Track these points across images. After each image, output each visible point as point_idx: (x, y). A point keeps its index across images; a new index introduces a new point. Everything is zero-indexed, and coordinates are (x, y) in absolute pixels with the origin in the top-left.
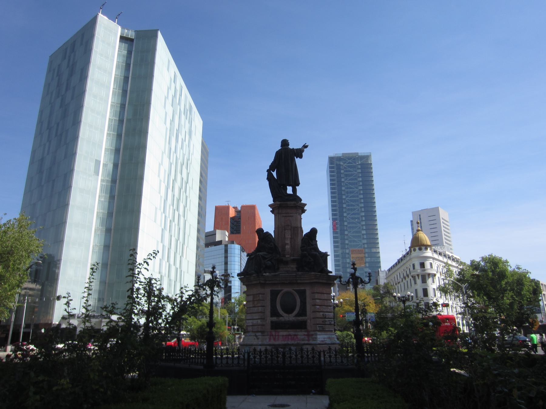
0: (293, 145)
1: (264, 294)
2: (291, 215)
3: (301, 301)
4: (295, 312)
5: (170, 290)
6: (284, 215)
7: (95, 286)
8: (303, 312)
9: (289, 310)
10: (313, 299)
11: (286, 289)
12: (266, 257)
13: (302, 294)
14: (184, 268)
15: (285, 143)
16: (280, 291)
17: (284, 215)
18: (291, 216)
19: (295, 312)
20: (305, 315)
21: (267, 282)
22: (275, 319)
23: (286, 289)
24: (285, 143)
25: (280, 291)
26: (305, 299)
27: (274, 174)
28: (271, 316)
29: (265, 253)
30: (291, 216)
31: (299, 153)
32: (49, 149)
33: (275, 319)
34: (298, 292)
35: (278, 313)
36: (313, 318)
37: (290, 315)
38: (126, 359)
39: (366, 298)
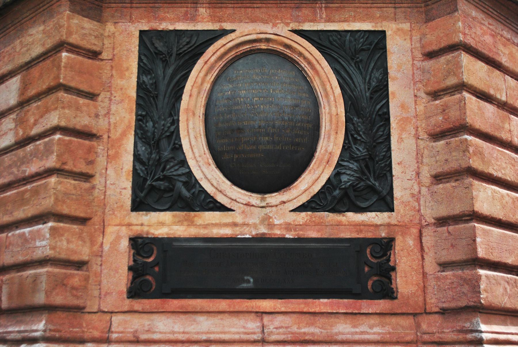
1: (94, 55)
3: (352, 105)
4: (313, 180)
7: (276, 237)
8: (365, 180)
9: (263, 161)
11: (245, 30)
13: (360, 59)
19: (313, 180)
20: (386, 203)
22: (163, 224)
26: (382, 90)
28: (139, 205)
32: (512, 334)
33: (163, 224)
34: (197, 201)
35: (190, 181)
36: (442, 221)
37: (274, 198)
38: (366, 269)
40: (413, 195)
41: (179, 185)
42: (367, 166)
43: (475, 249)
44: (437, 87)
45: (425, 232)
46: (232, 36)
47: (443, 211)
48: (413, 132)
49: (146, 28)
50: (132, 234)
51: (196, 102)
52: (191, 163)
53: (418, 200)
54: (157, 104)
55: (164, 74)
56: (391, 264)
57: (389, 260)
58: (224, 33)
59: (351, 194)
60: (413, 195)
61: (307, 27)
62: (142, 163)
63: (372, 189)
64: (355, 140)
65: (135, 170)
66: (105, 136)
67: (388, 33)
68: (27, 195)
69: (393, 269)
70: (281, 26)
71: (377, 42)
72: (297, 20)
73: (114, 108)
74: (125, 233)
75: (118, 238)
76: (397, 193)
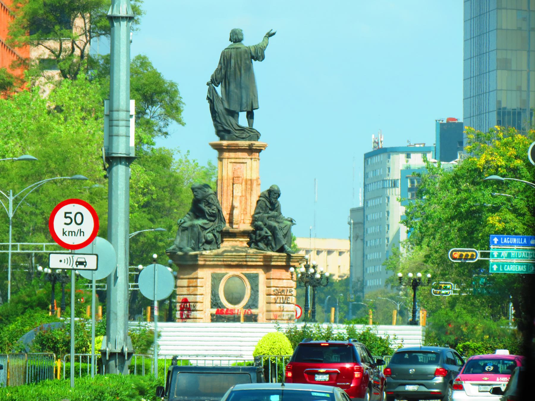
0: (250, 41)
2: (244, 161)
3: (252, 288)
4: (244, 302)
5: (201, 164)
6: (233, 161)
10: (268, 287)
12: (206, 227)
13: (253, 279)
14: (225, 188)
15: (236, 37)
16: (223, 275)
17: (233, 161)
18: (243, 163)
19: (244, 302)
21: (208, 263)
23: (231, 272)
24: (236, 37)
25: (223, 275)
26: (257, 285)
27: (219, 89)
29: (205, 221)
30: (243, 163)
31: (258, 55)
34: (248, 276)
39: (18, 188)
61: (243, 272)
71: (256, 276)
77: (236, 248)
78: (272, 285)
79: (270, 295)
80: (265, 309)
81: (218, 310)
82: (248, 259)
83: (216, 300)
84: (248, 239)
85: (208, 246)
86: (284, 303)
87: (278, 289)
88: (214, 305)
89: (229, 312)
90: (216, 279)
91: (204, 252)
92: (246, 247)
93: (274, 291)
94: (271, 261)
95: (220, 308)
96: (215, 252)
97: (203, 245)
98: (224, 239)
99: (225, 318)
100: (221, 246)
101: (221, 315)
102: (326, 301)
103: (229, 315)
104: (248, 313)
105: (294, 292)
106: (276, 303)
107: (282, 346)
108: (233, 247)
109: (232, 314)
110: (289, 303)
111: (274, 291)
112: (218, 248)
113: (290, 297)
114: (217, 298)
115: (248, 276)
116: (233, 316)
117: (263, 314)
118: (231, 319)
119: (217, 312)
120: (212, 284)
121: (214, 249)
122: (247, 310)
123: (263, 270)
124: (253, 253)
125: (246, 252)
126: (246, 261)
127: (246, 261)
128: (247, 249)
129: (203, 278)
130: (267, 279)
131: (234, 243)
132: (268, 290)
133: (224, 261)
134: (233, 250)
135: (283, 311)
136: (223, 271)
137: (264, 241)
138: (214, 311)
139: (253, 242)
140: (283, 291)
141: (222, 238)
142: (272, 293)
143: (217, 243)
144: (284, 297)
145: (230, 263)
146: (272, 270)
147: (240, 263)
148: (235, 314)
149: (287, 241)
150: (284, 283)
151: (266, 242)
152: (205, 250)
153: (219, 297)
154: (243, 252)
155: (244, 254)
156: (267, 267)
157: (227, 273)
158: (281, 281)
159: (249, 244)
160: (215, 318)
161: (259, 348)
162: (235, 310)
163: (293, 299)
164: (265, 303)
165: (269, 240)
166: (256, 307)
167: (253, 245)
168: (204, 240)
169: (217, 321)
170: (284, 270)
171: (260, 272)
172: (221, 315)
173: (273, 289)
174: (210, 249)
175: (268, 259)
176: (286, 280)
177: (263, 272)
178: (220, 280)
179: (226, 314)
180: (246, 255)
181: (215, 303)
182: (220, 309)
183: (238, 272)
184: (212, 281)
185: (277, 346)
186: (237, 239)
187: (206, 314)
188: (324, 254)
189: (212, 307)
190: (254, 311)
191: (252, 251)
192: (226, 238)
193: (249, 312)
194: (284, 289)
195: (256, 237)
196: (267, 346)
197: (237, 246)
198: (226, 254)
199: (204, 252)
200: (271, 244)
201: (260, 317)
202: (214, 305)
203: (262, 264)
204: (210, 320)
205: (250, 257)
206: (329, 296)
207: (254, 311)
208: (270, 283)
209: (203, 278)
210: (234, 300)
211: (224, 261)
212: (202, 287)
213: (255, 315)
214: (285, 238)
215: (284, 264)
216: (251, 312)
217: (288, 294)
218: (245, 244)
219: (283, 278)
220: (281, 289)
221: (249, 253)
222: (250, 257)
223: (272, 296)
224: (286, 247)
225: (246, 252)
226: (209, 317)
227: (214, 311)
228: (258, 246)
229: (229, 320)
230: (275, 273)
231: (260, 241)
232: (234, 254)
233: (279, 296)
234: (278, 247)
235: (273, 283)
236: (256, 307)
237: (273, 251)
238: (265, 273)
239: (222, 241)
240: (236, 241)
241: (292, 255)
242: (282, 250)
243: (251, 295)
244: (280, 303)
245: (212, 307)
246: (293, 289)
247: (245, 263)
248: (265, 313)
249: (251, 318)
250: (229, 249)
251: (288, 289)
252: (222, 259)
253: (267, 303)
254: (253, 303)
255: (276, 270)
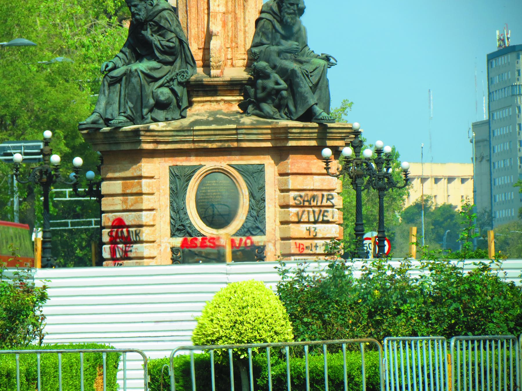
3: (252, 195)
13: (253, 176)
16: (194, 169)
23: (210, 163)
25: (194, 169)
26: (262, 188)
34: (242, 170)
40: (273, 229)
41: (187, 228)
42: (256, 219)
43: (290, 251)
44: (283, 188)
45: (277, 243)
46: (204, 167)
47: (283, 236)
48: (274, 205)
49: (171, 165)
50: (171, 246)
51: (245, 41)
52: (191, 219)
53: (275, 231)
54: (177, 194)
55: (207, 47)
56: (265, 255)
57: (264, 254)
58: (201, 166)
59: (251, 229)
60: (273, 229)
61: (233, 163)
62: (173, 219)
63: (258, 228)
64: (252, 209)
65: (171, 222)
66: (159, 209)
67: (265, 165)
68: (259, 382)
69: (265, 257)
70: (223, 163)
71: (260, 170)
72: (229, 160)
73: (161, 198)
74: (169, 247)
75: (166, 248)
76: (267, 228)
77: (218, 116)
78: (290, 187)
79: (287, 206)
80: (278, 237)
81: (185, 240)
82: (241, 137)
83: (180, 220)
84: (242, 98)
85: (160, 114)
86: (315, 222)
87: (303, 194)
88: (178, 230)
89: (208, 243)
90: (179, 179)
91: (153, 126)
92: (238, 113)
93: (295, 199)
94: (287, 139)
95: (190, 235)
96: (176, 124)
97: (151, 111)
98: (194, 99)
99: (199, 254)
100: (189, 112)
101: (193, 249)
102: (445, 237)
103: (208, 250)
104: (246, 243)
105: (338, 201)
106: (299, 222)
107: (262, 316)
108: (213, 114)
109: (215, 246)
110: (328, 222)
111: (295, 199)
112: (183, 117)
113: (330, 209)
114: (182, 216)
115: (242, 170)
116: (215, 251)
117: (275, 245)
118: (212, 257)
119: (184, 244)
120: (171, 189)
121: (173, 119)
122: (244, 239)
123: (273, 158)
124: (252, 124)
125: (237, 122)
126: (238, 141)
127: (238, 141)
128: (238, 116)
129: (152, 178)
130: (281, 175)
131: (214, 107)
132: (284, 197)
133: (194, 142)
134: (211, 119)
135: (315, 238)
136: (193, 161)
137: (273, 100)
138: (178, 241)
139: (250, 102)
140: (314, 197)
141: (190, 96)
142: (292, 202)
143: (179, 107)
144: (317, 210)
145: (205, 145)
146: (291, 156)
147: (226, 145)
148: (219, 246)
149: (319, 99)
150: (316, 182)
151: (277, 101)
152: (155, 120)
153: (186, 213)
154: (230, 122)
155: (234, 126)
156: (280, 152)
157: (201, 166)
158: (309, 177)
159: (243, 106)
160: (180, 256)
161: (206, 322)
162: (219, 238)
163: (335, 215)
164: (278, 223)
165: (282, 98)
166: (263, 232)
167: (250, 108)
168: (152, 101)
169: (184, 262)
170: (314, 157)
171: (268, 162)
172: (193, 249)
173: (292, 194)
174: (167, 120)
175: (281, 135)
176: (320, 178)
177: (272, 162)
178: (189, 180)
179: (203, 246)
180: (236, 129)
181: (180, 226)
182: (189, 238)
183: (222, 162)
184: (171, 182)
185: (250, 317)
186: (219, 98)
187: (162, 248)
188: (444, 182)
189: (173, 235)
190: (257, 239)
191: (247, 120)
192: (198, 96)
193: (249, 241)
194: (315, 193)
195: (256, 93)
196: (226, 318)
197: (219, 112)
198: (196, 128)
199: (153, 126)
200: (287, 106)
201: (270, 251)
202: (178, 230)
203: (269, 144)
204: (170, 262)
205: (244, 131)
206: (449, 231)
207: (257, 239)
208: (286, 183)
209: (152, 178)
210: (217, 219)
211: (194, 142)
212: (152, 194)
213: (259, 247)
214: (314, 93)
215: (313, 143)
216: (252, 243)
217: (324, 203)
218: (236, 108)
219: (314, 171)
220: (310, 193)
221: (243, 124)
222: (244, 131)
223: (291, 209)
224: (318, 109)
225: (237, 122)
226: (169, 254)
227: (178, 241)
228: (261, 110)
229: (208, 259)
230: (295, 163)
231: (264, 100)
232: (213, 127)
233: (307, 209)
234: (301, 113)
235: (293, 182)
236: (263, 232)
237: (292, 119)
238: (277, 163)
239: (191, 104)
240: (217, 101)
241: (330, 125)
242: (308, 116)
243: (251, 208)
244: (309, 222)
245: (173, 235)
246: (334, 193)
247: (235, 144)
248: (279, 243)
249: (256, 254)
250: (204, 118)
251: (325, 193)
252: (191, 138)
253: (282, 223)
254: (256, 224)
255: (299, 156)
